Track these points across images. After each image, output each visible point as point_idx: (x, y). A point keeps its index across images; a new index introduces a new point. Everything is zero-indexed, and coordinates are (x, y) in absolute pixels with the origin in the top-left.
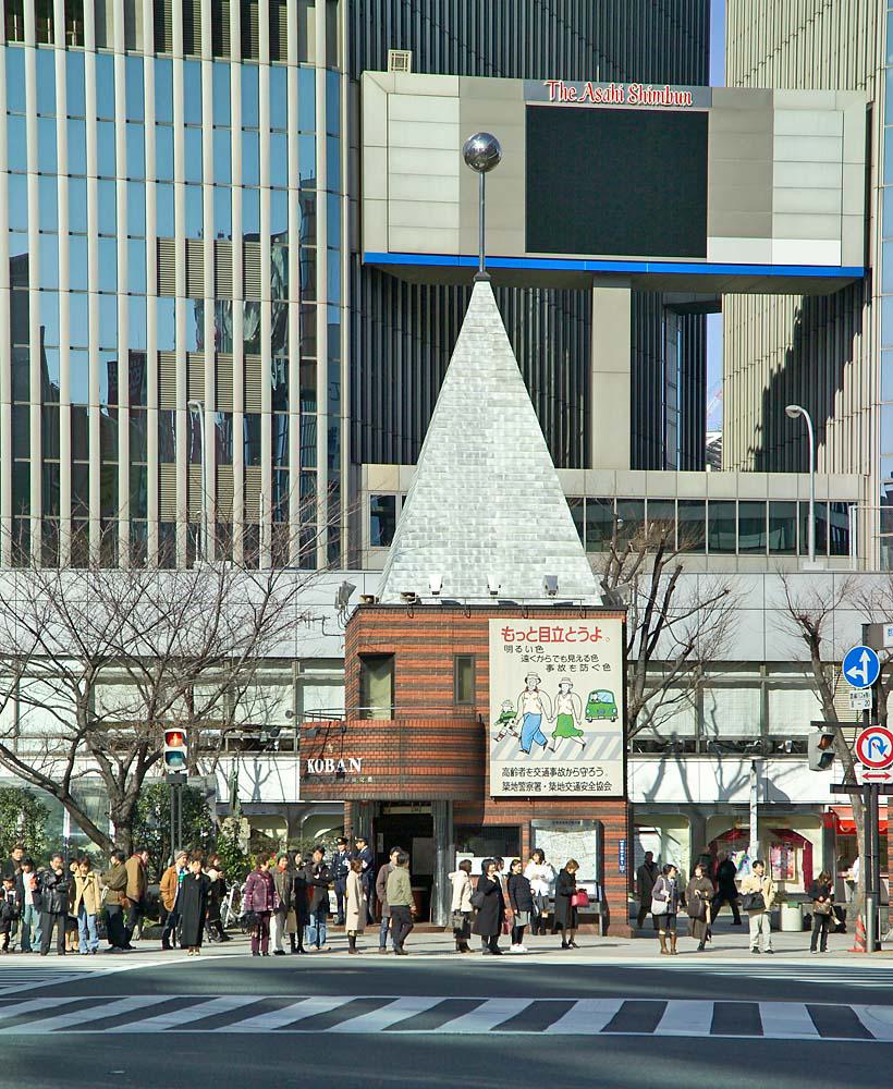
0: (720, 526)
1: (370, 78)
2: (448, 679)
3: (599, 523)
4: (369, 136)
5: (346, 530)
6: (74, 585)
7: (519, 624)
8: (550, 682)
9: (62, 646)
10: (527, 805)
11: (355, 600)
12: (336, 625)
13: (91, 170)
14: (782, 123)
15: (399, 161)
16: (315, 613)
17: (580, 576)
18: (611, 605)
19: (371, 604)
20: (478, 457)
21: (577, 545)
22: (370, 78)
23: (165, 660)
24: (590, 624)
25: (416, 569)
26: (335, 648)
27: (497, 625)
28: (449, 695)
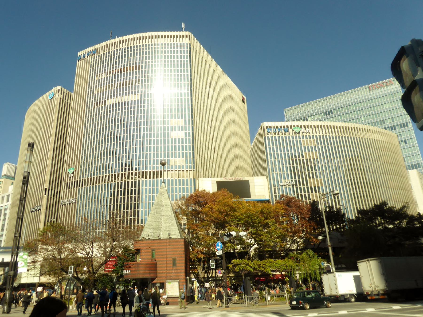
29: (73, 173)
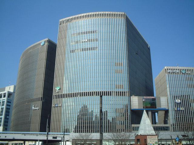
0: (159, 129)
1: (131, 97)
2: (144, 141)
3: (156, 129)
4: (131, 104)
5: (168, 87)
6: (115, 134)
7: (149, 136)
8: (152, 141)
9: (49, 134)
10: (38, 91)
11: (136, 135)
12: (134, 137)
13: (107, 84)
14: (161, 99)
15: (134, 106)
16: (132, 136)
17: (153, 132)
18: (156, 135)
19: (137, 135)
20: (145, 123)
21: (153, 130)
22: (131, 97)
23: (120, 140)
24: (155, 136)
25: (141, 132)
26: (134, 138)
27: (148, 136)
28: (144, 142)
29: (59, 90)
